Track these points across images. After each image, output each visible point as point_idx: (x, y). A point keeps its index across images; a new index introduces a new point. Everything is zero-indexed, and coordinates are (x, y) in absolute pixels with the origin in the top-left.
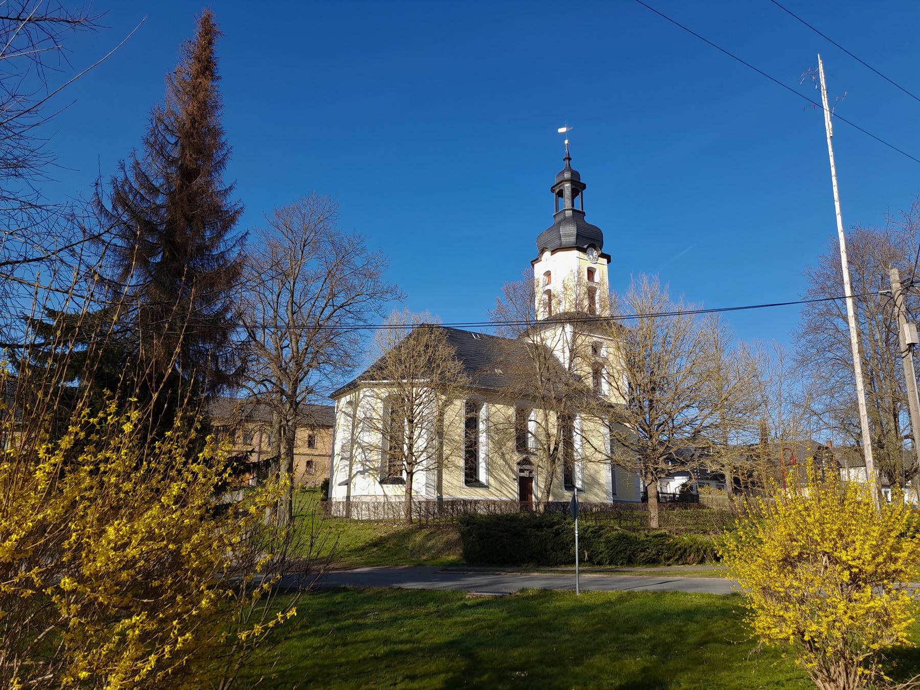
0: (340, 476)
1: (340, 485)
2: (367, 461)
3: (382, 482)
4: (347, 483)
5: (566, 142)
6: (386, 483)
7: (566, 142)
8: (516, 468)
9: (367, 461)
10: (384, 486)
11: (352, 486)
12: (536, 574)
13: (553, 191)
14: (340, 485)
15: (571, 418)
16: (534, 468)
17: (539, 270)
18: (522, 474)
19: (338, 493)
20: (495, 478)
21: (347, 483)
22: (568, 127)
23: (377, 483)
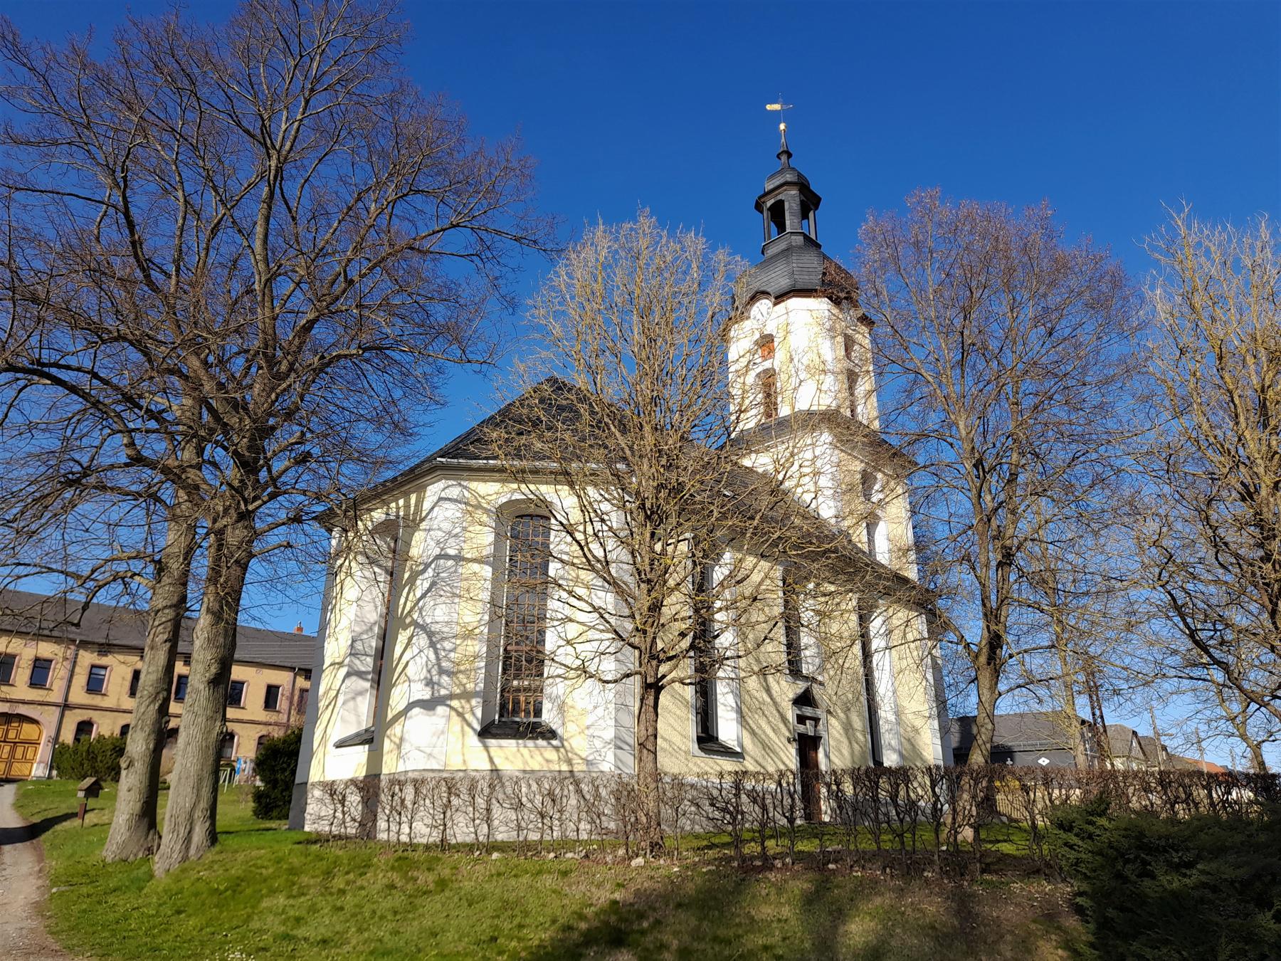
0: (341, 711)
1: (340, 745)
2: (442, 671)
3: (486, 732)
4: (370, 739)
5: (782, 126)
6: (495, 736)
7: (782, 126)
8: (791, 714)
9: (442, 671)
10: (492, 742)
11: (387, 745)
12: (402, 600)
13: (759, 207)
14: (340, 745)
15: (872, 608)
16: (820, 713)
17: (741, 343)
18: (801, 728)
19: (332, 763)
20: (753, 733)
21: (370, 739)
22: (784, 103)
23: (473, 739)
